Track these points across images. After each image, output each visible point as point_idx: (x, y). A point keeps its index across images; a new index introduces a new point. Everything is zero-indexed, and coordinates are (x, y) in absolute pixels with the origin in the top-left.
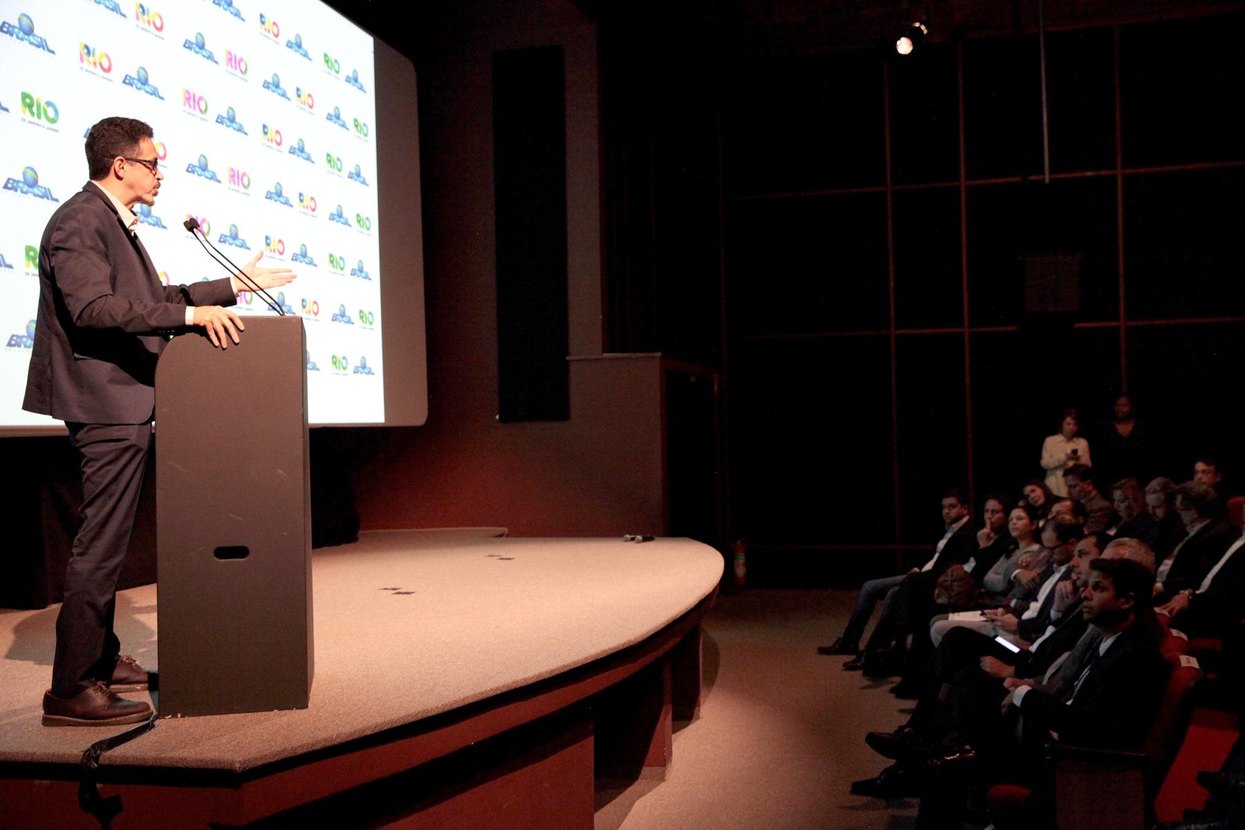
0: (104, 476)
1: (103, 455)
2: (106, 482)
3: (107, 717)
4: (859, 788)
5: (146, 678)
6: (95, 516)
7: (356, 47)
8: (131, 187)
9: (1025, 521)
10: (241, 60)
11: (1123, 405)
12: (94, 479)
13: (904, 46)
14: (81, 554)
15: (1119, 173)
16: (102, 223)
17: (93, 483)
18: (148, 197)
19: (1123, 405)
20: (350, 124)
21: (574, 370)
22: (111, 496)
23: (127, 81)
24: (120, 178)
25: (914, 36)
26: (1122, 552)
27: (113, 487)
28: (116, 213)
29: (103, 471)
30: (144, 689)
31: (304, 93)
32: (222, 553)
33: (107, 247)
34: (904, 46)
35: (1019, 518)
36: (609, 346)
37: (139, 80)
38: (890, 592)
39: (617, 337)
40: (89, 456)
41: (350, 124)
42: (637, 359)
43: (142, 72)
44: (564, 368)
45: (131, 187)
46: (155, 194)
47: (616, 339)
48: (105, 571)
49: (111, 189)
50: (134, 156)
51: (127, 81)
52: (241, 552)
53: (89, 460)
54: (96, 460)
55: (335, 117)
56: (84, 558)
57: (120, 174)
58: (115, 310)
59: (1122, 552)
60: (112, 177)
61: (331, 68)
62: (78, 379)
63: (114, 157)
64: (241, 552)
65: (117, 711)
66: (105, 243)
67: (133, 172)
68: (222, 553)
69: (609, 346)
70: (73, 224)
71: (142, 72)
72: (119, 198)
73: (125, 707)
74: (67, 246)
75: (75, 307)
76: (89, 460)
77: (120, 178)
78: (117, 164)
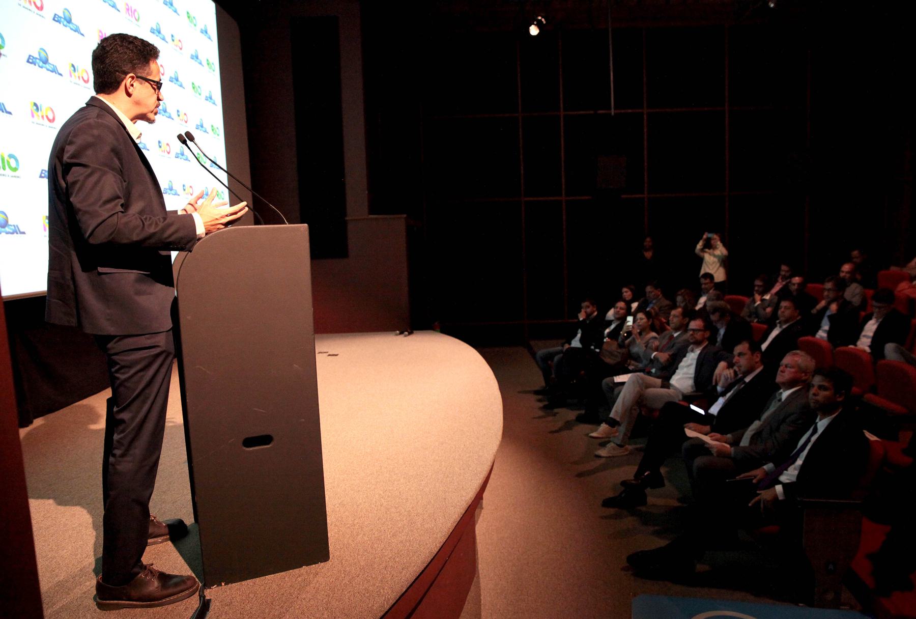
0: (139, 382)
1: (136, 362)
2: (141, 387)
3: (157, 600)
4: (607, 503)
5: (166, 531)
6: (133, 418)
7: (213, 5)
8: (137, 103)
9: (645, 320)
10: (135, 10)
11: (648, 241)
12: (128, 384)
13: (534, 31)
14: (123, 456)
15: (645, 111)
16: (117, 140)
17: (125, 387)
18: (151, 116)
19: (648, 241)
20: (204, 63)
21: (350, 226)
22: (144, 402)
23: (56, 19)
24: (129, 95)
25: (539, 25)
26: (796, 359)
27: (147, 391)
28: (124, 128)
29: (136, 378)
30: (166, 540)
31: (176, 39)
32: (249, 442)
33: (121, 164)
34: (534, 31)
35: (641, 319)
36: (371, 212)
37: (65, 19)
38: (556, 358)
39: (379, 204)
40: (123, 364)
41: (204, 63)
42: (376, 219)
43: (67, 13)
44: (345, 223)
45: (137, 103)
46: (156, 114)
47: (375, 207)
48: (147, 468)
49: (117, 104)
50: (144, 75)
51: (56, 19)
52: (266, 439)
53: (122, 367)
54: (130, 367)
55: (195, 57)
56: (125, 459)
57: (130, 91)
58: (132, 225)
59: (796, 359)
60: (121, 92)
61: (191, 22)
62: (105, 295)
63: (126, 73)
64: (266, 439)
65: (170, 591)
66: (120, 159)
67: (141, 90)
68: (249, 442)
69: (371, 212)
70: (80, 141)
71: (67, 13)
72: (125, 113)
73: (176, 585)
74: (83, 160)
75: (89, 224)
76: (122, 367)
77: (129, 95)
78: (128, 81)
